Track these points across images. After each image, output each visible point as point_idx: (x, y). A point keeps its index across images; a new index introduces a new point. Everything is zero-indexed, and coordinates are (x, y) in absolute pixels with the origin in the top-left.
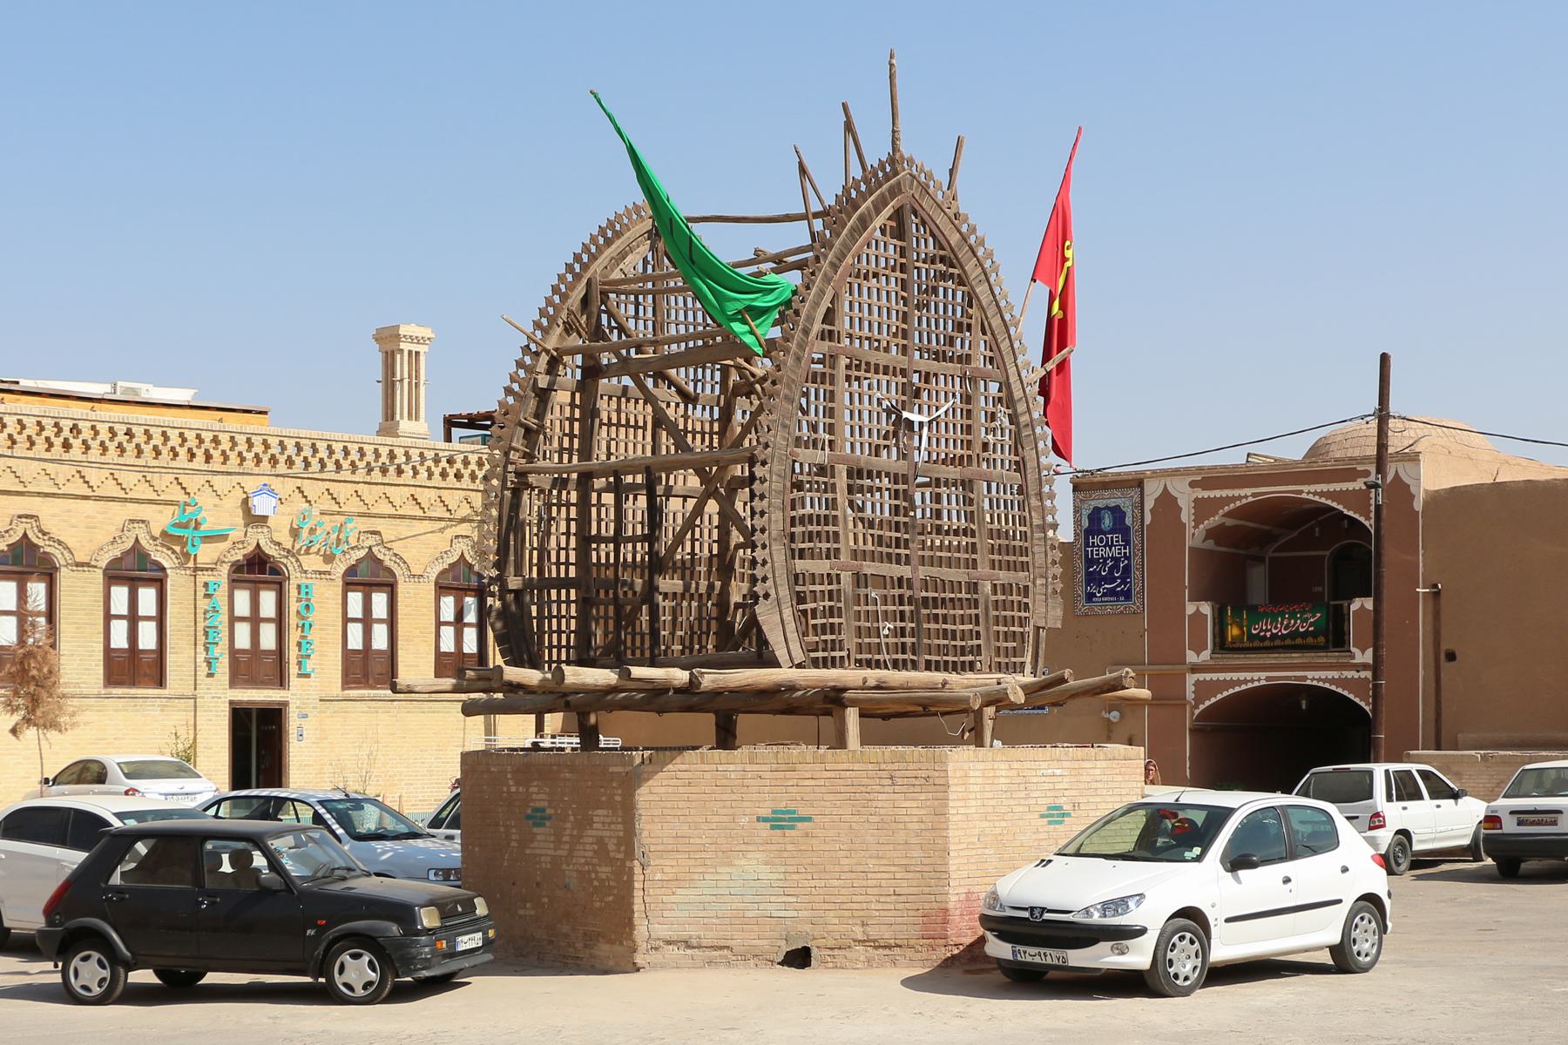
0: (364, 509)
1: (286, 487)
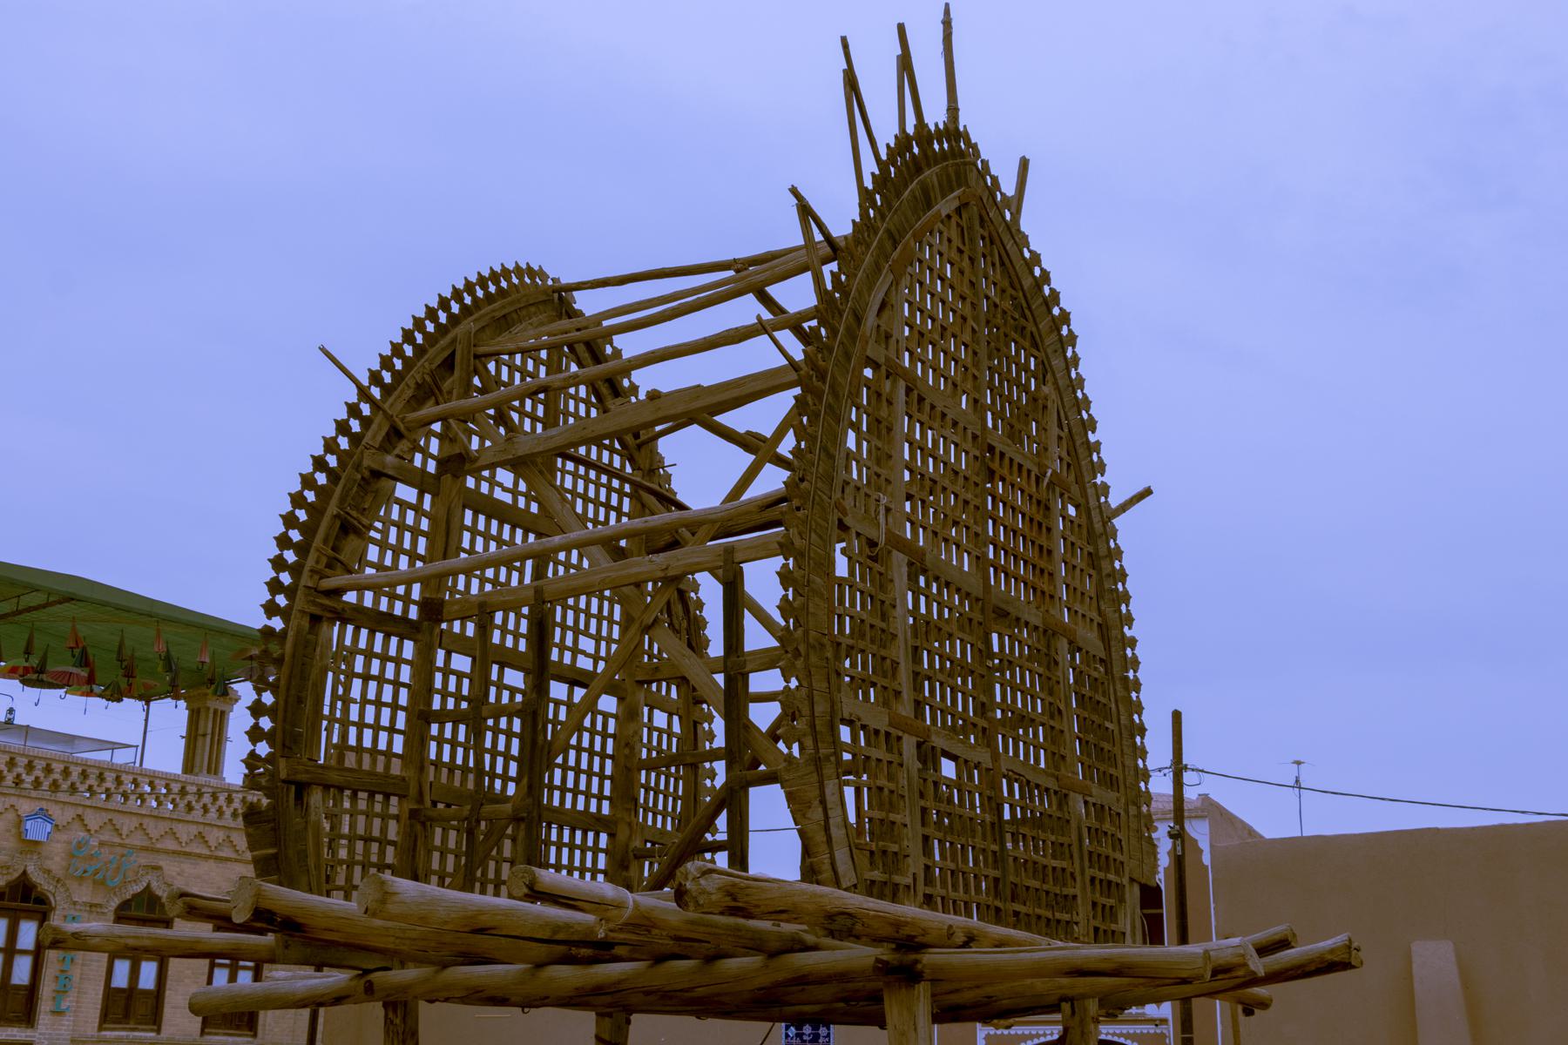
0: (146, 843)
1: (62, 815)
